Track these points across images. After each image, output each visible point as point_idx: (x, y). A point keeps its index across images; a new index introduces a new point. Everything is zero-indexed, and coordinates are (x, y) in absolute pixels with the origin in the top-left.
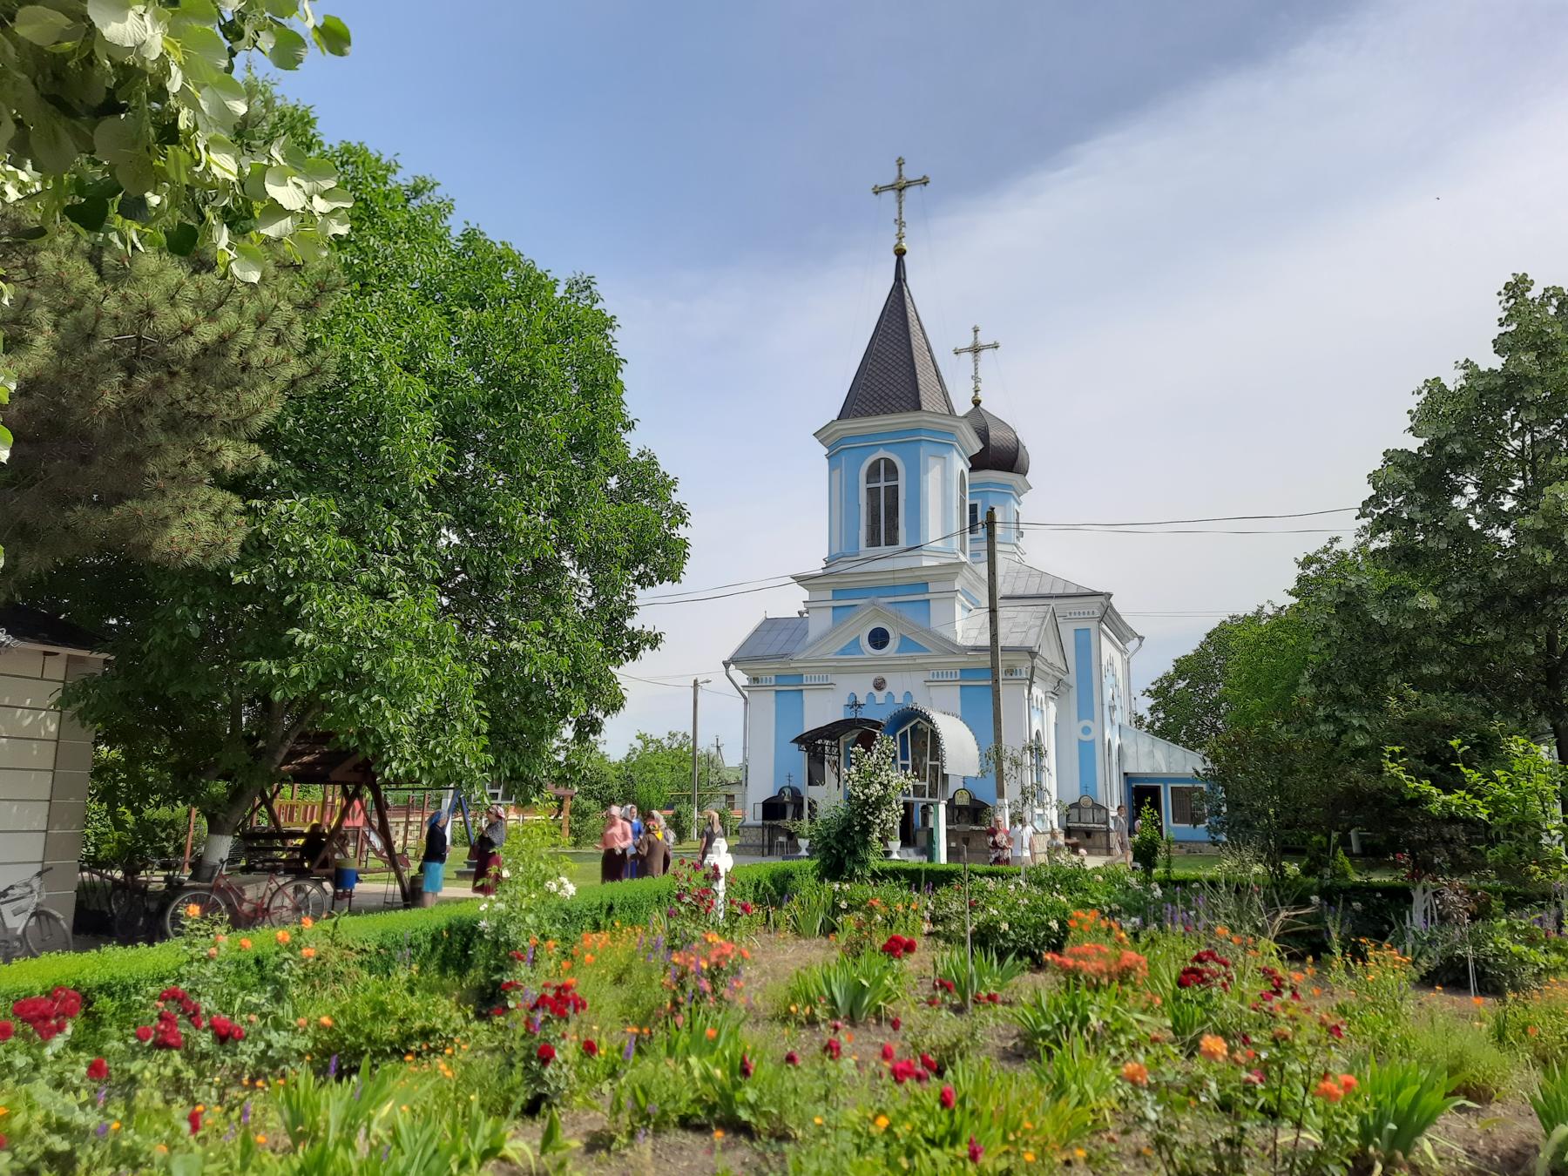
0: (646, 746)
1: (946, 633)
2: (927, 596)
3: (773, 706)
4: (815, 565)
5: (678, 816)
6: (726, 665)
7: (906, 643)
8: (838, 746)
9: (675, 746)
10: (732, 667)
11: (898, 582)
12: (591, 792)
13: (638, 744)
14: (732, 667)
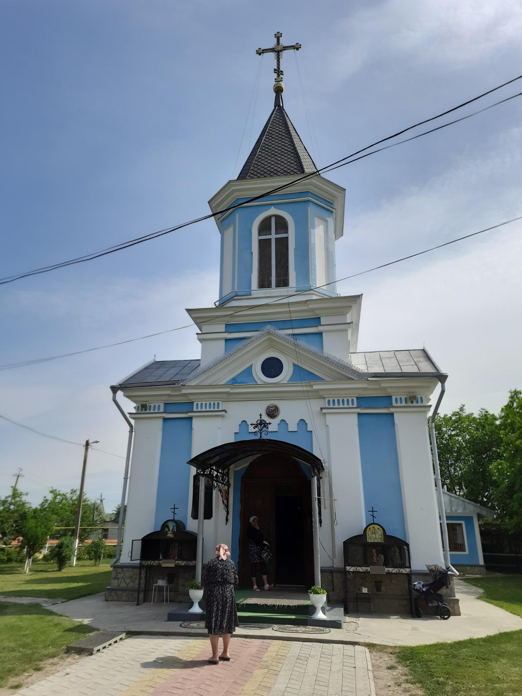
0: (55, 498)
2: (320, 329)
3: (160, 434)
5: (60, 546)
6: (115, 389)
7: (300, 373)
8: (228, 474)
11: (295, 316)
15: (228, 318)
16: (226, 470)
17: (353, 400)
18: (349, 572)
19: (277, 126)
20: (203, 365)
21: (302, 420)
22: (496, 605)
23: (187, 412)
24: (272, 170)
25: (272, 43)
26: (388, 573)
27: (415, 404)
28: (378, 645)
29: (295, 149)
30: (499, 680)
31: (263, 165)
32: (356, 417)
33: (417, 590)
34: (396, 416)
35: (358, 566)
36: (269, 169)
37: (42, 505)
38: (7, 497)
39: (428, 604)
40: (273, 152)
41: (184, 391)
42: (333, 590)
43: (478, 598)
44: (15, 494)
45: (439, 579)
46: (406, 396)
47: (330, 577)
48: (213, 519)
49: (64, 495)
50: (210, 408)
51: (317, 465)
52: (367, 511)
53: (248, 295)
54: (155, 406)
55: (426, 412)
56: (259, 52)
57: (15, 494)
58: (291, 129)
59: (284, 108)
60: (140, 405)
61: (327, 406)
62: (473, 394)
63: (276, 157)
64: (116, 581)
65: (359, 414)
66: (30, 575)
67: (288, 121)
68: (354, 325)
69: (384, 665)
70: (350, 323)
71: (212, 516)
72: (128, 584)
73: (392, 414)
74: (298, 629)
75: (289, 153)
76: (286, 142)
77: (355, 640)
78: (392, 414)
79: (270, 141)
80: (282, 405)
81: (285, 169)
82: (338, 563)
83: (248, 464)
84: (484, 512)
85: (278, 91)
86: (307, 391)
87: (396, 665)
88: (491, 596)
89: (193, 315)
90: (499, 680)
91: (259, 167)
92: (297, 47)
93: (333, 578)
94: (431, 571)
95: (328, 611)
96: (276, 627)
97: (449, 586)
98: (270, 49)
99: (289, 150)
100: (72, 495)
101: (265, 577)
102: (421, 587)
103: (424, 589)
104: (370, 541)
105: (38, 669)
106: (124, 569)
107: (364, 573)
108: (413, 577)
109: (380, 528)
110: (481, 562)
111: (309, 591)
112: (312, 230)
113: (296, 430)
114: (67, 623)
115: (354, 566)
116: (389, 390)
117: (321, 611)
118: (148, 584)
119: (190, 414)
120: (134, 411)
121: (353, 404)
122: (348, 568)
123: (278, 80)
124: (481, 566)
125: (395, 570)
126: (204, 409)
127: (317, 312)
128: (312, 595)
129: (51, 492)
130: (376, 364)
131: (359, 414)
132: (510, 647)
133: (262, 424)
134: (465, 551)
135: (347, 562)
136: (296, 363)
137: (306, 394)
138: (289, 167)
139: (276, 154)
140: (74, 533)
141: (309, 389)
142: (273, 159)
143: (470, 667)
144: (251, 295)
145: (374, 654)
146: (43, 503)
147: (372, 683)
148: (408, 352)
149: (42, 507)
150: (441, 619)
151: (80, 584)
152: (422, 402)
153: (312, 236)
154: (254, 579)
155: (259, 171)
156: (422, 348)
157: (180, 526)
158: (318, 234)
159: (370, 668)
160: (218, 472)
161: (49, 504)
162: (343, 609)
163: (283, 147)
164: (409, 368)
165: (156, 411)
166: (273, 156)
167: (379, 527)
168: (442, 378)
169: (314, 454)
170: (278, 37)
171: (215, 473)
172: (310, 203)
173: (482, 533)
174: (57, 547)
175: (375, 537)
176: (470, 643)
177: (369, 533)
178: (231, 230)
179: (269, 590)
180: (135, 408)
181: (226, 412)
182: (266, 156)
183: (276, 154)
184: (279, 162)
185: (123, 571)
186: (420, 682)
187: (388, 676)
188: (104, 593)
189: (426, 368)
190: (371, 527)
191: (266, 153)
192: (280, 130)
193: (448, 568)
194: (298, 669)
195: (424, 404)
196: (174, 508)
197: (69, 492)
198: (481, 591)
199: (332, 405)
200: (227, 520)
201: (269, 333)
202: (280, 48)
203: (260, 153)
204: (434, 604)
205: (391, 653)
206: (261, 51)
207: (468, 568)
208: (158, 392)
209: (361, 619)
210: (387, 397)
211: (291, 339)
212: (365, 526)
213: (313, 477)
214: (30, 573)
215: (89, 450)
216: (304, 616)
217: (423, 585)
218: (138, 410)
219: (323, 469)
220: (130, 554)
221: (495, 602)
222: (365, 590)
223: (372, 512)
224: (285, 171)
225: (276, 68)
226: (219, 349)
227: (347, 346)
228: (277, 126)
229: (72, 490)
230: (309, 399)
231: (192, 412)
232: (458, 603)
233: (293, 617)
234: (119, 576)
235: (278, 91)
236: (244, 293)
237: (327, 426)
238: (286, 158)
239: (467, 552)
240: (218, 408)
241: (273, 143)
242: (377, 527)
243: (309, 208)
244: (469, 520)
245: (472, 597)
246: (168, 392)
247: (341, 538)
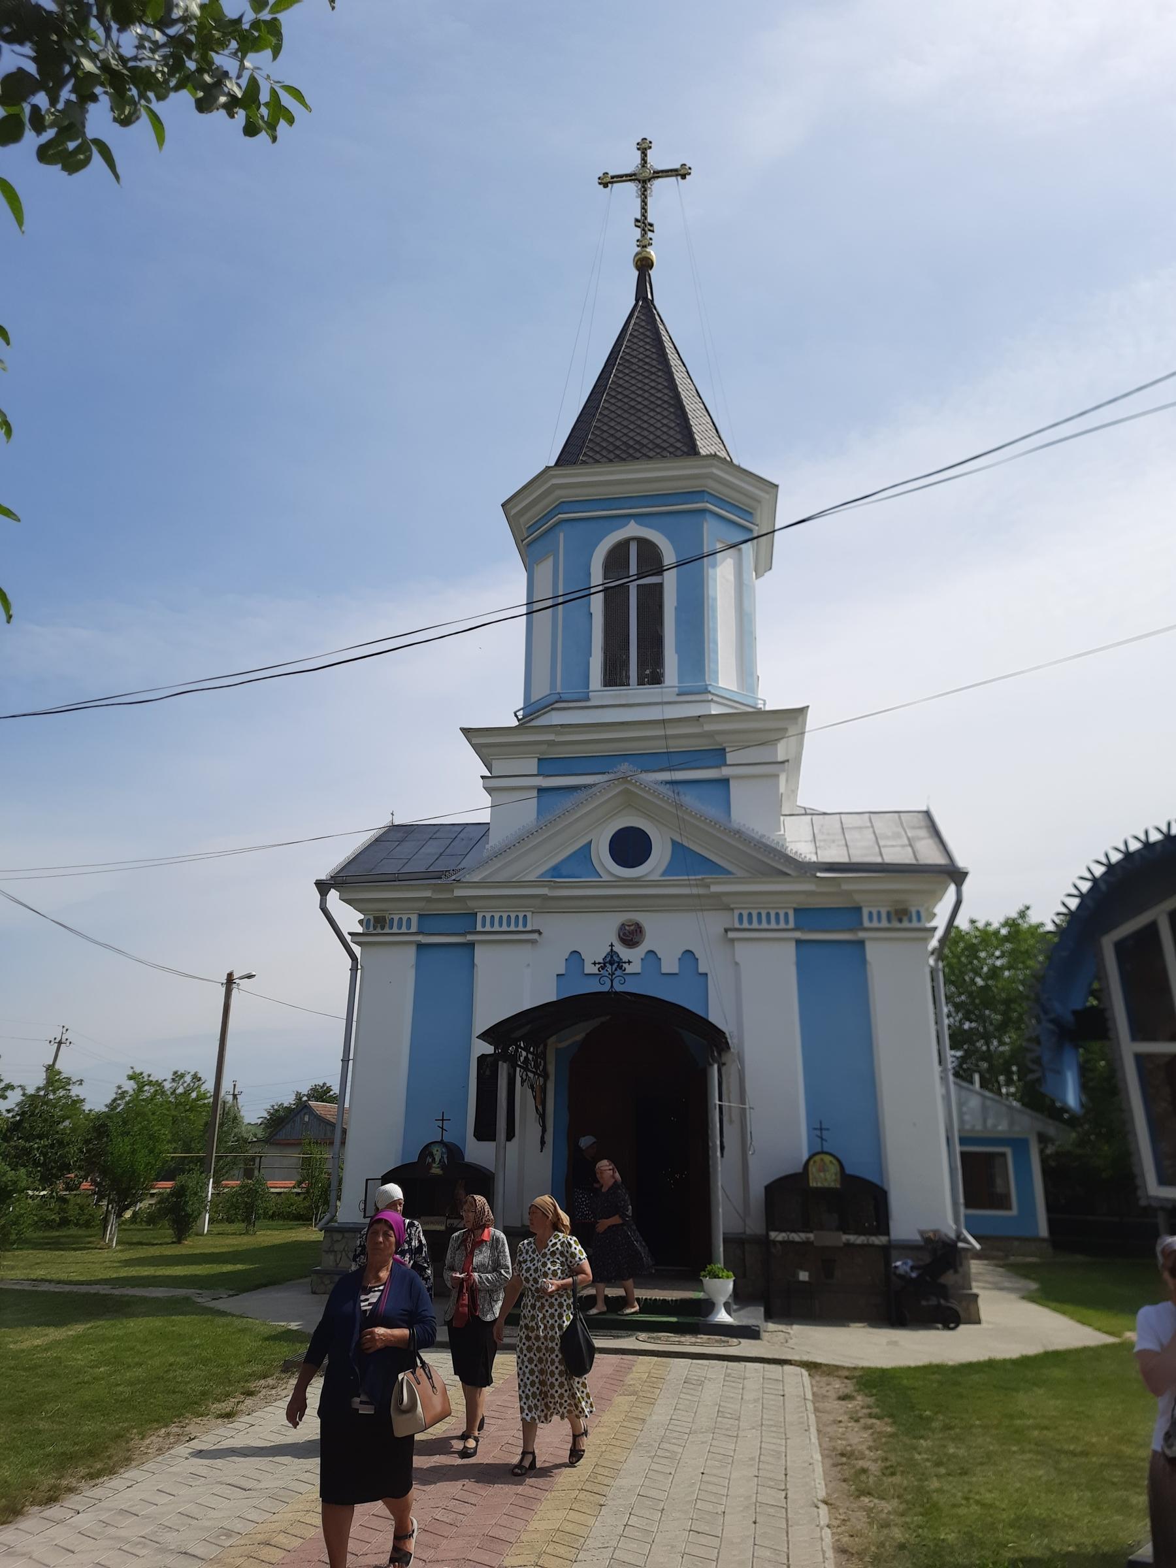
0: (140, 1090)
1: (772, 838)
2: (725, 772)
3: (411, 974)
4: (502, 710)
5: (179, 1192)
6: (323, 887)
7: (685, 859)
8: (543, 1055)
9: (180, 1090)
10: (333, 895)
11: (675, 746)
12: (27, 1152)
13: (130, 1086)
14: (333, 895)
15: (544, 747)
17: (786, 915)
18: (774, 1242)
19: (641, 344)
20: (495, 840)
21: (688, 951)
22: (1055, 1310)
23: (464, 934)
24: (631, 443)
25: (630, 162)
26: (848, 1245)
27: (906, 924)
28: (826, 1365)
29: (677, 396)
30: (1022, 1415)
31: (612, 432)
32: (792, 946)
33: (901, 1277)
36: (625, 439)
37: (112, 1106)
38: (39, 1089)
40: (633, 403)
41: (458, 893)
43: (1023, 1298)
44: (53, 1077)
45: (942, 1256)
46: (889, 909)
49: (158, 1084)
50: (509, 925)
51: (715, 1041)
52: (811, 1128)
53: (582, 699)
55: (926, 941)
56: (605, 181)
57: (53, 1077)
58: (670, 350)
59: (655, 303)
60: (371, 917)
61: (737, 925)
63: (639, 414)
64: (332, 1257)
65: (799, 942)
66: (121, 1251)
67: (663, 333)
68: (791, 765)
69: (833, 1395)
70: (783, 762)
73: (861, 943)
74: (683, 1339)
75: (666, 406)
76: (660, 380)
77: (783, 1357)
78: (861, 943)
79: (627, 378)
80: (651, 923)
81: (658, 441)
82: (755, 1225)
83: (583, 1035)
84: (1051, 1129)
85: (644, 265)
86: (699, 896)
87: (855, 1394)
88: (1051, 1295)
90: (1022, 1415)
91: (605, 435)
92: (682, 173)
94: (928, 1240)
95: (735, 1311)
96: (643, 1336)
97: (960, 1270)
98: (626, 175)
99: (666, 398)
100: (175, 1085)
103: (914, 1275)
105: (250, 1394)
106: (346, 1235)
108: (894, 1253)
109: (835, 1161)
110: (1043, 1231)
111: (703, 1273)
112: (711, 571)
113: (676, 971)
114: (265, 1330)
115: (785, 1231)
116: (857, 897)
117: (723, 1310)
119: (470, 938)
120: (360, 930)
121: (787, 922)
122: (773, 1235)
123: (643, 244)
124: (1043, 1240)
125: (860, 1240)
126: (496, 928)
127: (719, 738)
128: (707, 1281)
129: (130, 1078)
130: (834, 841)
131: (799, 942)
132: (1057, 1373)
133: (612, 961)
134: (1009, 1208)
135: (772, 1222)
138: (665, 437)
139: (639, 407)
140: (203, 1163)
141: (701, 891)
142: (633, 418)
143: (980, 1398)
144: (588, 699)
145: (818, 1378)
146: (115, 1100)
147: (812, 1418)
148: (896, 815)
149: (112, 1110)
151: (240, 1267)
152: (919, 919)
153: (711, 582)
155: (604, 444)
156: (925, 809)
157: (454, 1152)
158: (722, 575)
159: (809, 1396)
160: (528, 1052)
161: (127, 1103)
162: (762, 1309)
163: (652, 391)
164: (897, 854)
165: (404, 930)
166: (632, 411)
167: (831, 1158)
168: (957, 876)
169: (711, 1019)
170: (644, 148)
171: (524, 1053)
172: (708, 516)
173: (1046, 1172)
174: (172, 1194)
175: (825, 1178)
176: (990, 1365)
177: (813, 1169)
178: (549, 563)
180: (361, 922)
181: (540, 933)
182: (619, 412)
183: (639, 407)
184: (645, 425)
186: (891, 1416)
187: (839, 1409)
188: (308, 1280)
189: (930, 855)
190: (817, 1158)
191: (619, 404)
192: (648, 353)
193: (960, 1237)
194: (689, 1397)
197: (170, 1076)
198: (1034, 1286)
200: (543, 1143)
201: (624, 779)
202: (646, 175)
203: (606, 405)
205: (847, 1378)
206: (608, 180)
207: (1016, 1243)
208: (401, 887)
209: (795, 1327)
210: (852, 910)
211: (664, 790)
212: (805, 1157)
213: (711, 1065)
214: (119, 1248)
215: (235, 992)
216: (692, 1318)
218: (368, 927)
219: (729, 1048)
220: (362, 1206)
221: (1054, 1305)
222: (804, 1276)
223: (818, 1130)
224: (658, 446)
225: (639, 217)
226: (526, 811)
227: (775, 808)
228: (641, 344)
229: (175, 1073)
233: (674, 1319)
234: (337, 1247)
235: (644, 265)
236: (575, 697)
237: (737, 964)
238: (659, 417)
239: (1014, 1212)
240: (525, 925)
241: (633, 382)
242: (828, 1158)
243: (705, 526)
244: (1019, 1145)
245: (1013, 1296)
246: (428, 894)
247: (760, 1177)
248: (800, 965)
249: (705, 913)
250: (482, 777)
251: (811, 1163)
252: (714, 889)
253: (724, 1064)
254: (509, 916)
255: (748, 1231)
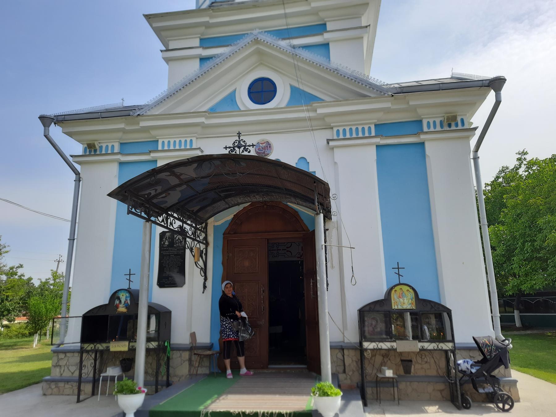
7: (299, 96)
15: (202, 29)
16: (204, 225)
17: (370, 128)
21: (303, 158)
26: (423, 350)
34: (427, 145)
35: (379, 342)
39: (478, 391)
41: (143, 124)
42: (344, 372)
46: (442, 119)
47: (340, 355)
48: (186, 286)
54: (107, 146)
55: (468, 138)
60: (86, 146)
61: (335, 137)
62: (505, 145)
64: (58, 370)
65: (378, 147)
70: (366, 27)
71: (185, 283)
72: (73, 373)
73: (422, 144)
82: (352, 336)
83: (232, 216)
86: (310, 119)
89: (155, 25)
93: (343, 356)
101: (242, 359)
102: (469, 367)
104: (396, 308)
106: (68, 355)
107: (389, 350)
109: (411, 290)
115: (374, 342)
118: (98, 370)
120: (80, 152)
122: (366, 345)
127: (322, 14)
131: (378, 147)
135: (363, 336)
136: (296, 84)
137: (309, 123)
141: (312, 114)
150: (498, 411)
152: (463, 124)
154: (228, 362)
167: (408, 288)
179: (253, 375)
185: (66, 356)
190: (397, 288)
195: (466, 127)
196: (130, 274)
199: (341, 137)
200: (205, 287)
204: (487, 390)
212: (385, 289)
217: (471, 365)
221: (532, 371)
222: (389, 373)
230: (312, 130)
231: (157, 151)
232: (516, 385)
234: (62, 363)
237: (335, 163)
242: (405, 288)
246: (122, 126)
248: (380, 162)
249: (315, 132)
250: (161, 51)
251: (393, 291)
252: (320, 111)
253: (327, 230)
254: (180, 141)
255: (346, 341)
